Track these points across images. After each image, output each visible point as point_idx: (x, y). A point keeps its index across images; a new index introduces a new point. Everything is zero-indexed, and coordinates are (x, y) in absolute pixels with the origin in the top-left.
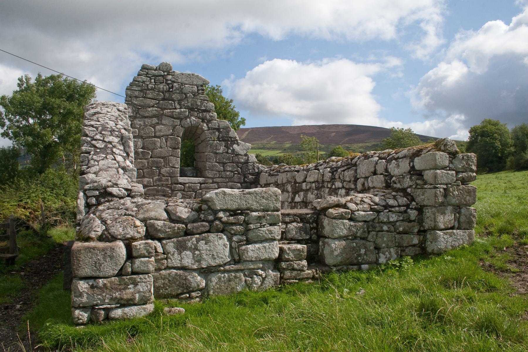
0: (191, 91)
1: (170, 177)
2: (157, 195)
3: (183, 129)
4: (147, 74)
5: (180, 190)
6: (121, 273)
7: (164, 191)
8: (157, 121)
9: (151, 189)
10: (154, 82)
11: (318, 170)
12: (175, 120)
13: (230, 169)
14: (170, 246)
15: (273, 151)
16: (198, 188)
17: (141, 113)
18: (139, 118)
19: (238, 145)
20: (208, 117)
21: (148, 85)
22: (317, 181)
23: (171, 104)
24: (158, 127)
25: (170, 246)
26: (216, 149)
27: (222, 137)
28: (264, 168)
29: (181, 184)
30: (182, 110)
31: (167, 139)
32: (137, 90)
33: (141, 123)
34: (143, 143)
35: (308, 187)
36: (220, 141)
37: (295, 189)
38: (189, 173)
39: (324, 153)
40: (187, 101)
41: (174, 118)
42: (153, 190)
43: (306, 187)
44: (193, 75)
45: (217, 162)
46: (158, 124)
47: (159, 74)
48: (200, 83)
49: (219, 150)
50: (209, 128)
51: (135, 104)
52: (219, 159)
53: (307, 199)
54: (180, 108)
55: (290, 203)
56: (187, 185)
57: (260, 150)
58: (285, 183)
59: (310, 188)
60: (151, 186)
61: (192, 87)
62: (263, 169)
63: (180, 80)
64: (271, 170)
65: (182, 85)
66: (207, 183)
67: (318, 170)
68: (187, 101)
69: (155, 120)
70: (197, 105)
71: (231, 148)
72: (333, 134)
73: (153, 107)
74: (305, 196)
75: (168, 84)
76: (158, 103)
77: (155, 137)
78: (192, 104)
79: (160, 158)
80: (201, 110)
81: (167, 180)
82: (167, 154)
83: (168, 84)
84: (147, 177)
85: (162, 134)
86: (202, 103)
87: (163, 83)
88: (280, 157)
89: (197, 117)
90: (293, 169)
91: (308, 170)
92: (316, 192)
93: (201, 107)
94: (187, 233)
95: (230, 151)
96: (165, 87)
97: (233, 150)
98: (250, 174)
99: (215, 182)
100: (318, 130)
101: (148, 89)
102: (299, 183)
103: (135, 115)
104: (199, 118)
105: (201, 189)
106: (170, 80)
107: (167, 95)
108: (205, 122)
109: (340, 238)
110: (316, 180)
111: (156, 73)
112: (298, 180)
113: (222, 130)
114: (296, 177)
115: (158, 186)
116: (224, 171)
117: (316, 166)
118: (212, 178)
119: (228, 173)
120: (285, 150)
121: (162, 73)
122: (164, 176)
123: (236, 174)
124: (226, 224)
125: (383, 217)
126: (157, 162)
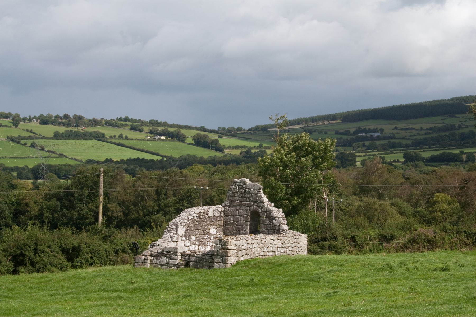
6: (143, 262)
14: (155, 258)
24: (240, 211)
25: (155, 258)
46: (240, 209)
69: (238, 208)
77: (238, 215)
86: (259, 198)
94: (159, 256)
97: (273, 223)
109: (192, 261)
124: (166, 255)
125: (204, 257)
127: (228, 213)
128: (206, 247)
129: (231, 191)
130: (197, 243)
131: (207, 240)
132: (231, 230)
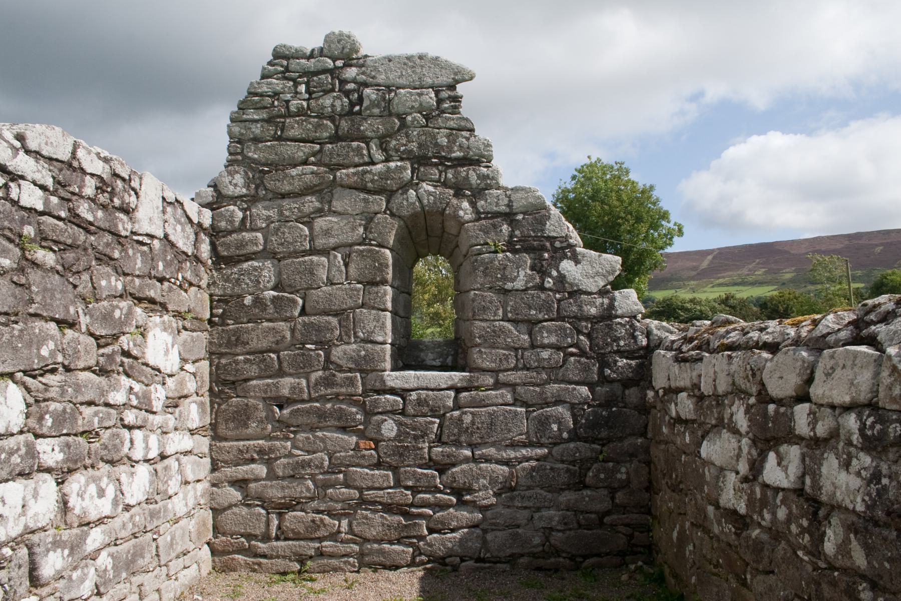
0: (416, 105)
1: (361, 371)
2: (321, 429)
3: (396, 224)
4: (287, 69)
5: (393, 412)
7: (341, 415)
8: (317, 204)
9: (302, 410)
10: (308, 91)
11: (872, 341)
12: (371, 198)
13: (553, 339)
15: (761, 288)
16: (450, 403)
17: (270, 184)
18: (264, 199)
19: (577, 262)
20: (474, 179)
21: (287, 102)
22: (872, 406)
23: (359, 149)
24: (321, 223)
26: (505, 278)
27: (523, 239)
28: (668, 331)
29: (393, 391)
30: (392, 165)
31: (349, 256)
32: (256, 121)
33: (271, 213)
34: (279, 274)
35: (821, 430)
36: (515, 252)
37: (763, 427)
38: (431, 356)
39: (861, 285)
40: (407, 136)
41: (369, 192)
42: (308, 412)
43: (813, 424)
44: (421, 57)
45: (509, 321)
46: (320, 212)
47: (320, 66)
48: (445, 78)
49: (513, 280)
50: (478, 213)
51: (254, 161)
52: (515, 310)
53: (817, 486)
54: (387, 160)
55: (745, 480)
56: (414, 396)
57: (736, 288)
58: (726, 395)
59: (834, 434)
60: (303, 401)
61: (420, 95)
62: (664, 334)
63: (381, 79)
64: (685, 338)
65: (390, 91)
66: (477, 388)
67: (872, 341)
68: (407, 136)
69: (311, 203)
70: (437, 145)
71: (554, 273)
72: (879, 249)
73: (305, 163)
74: (811, 469)
75: (347, 94)
76: (320, 151)
77: (313, 251)
78: (420, 146)
79: (327, 314)
80: (450, 160)
81: (351, 382)
82: (350, 303)
83: (347, 94)
84: (291, 375)
85: (332, 241)
87: (333, 90)
88: (772, 299)
89: (437, 183)
90: (755, 335)
91: (818, 344)
92: (866, 460)
93: (451, 151)
95: (549, 283)
96: (338, 103)
97: (561, 279)
98: (621, 353)
99: (505, 385)
100: (847, 242)
101: (289, 114)
102: (779, 402)
103: (253, 192)
104: (445, 184)
105: (457, 406)
106: (354, 81)
107: (344, 124)
108: (464, 196)
110: (863, 397)
111: (311, 64)
112: (776, 389)
113: (520, 217)
114: (765, 376)
115: (322, 399)
116: (533, 346)
117: (857, 324)
118: (495, 372)
119: (545, 354)
120: (784, 284)
121: (330, 63)
122: (340, 369)
123: (572, 354)
126: (319, 329)
127: (242, 244)
128: (122, 471)
129: (259, 108)
130: (50, 452)
131: (130, 417)
132: (264, 344)
